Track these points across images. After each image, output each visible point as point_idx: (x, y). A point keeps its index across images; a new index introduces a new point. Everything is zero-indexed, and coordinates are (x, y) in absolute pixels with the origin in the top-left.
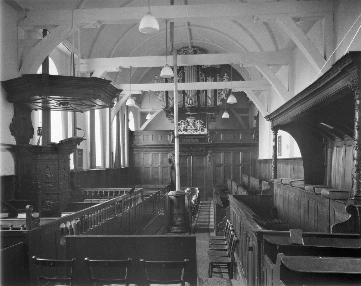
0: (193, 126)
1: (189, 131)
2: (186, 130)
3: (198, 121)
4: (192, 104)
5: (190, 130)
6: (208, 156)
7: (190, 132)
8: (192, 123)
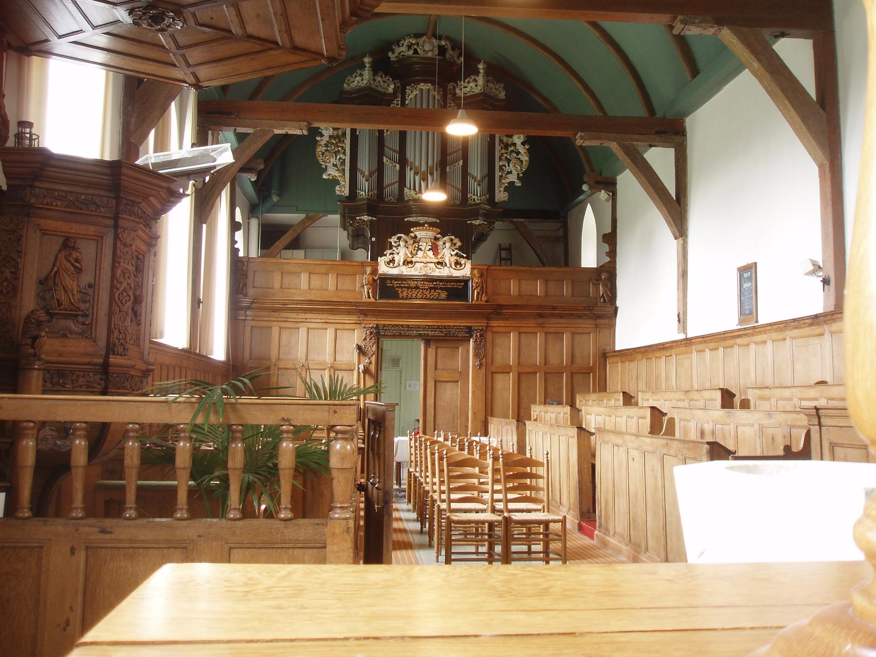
0: (431, 253)
2: (411, 262)
3: (446, 238)
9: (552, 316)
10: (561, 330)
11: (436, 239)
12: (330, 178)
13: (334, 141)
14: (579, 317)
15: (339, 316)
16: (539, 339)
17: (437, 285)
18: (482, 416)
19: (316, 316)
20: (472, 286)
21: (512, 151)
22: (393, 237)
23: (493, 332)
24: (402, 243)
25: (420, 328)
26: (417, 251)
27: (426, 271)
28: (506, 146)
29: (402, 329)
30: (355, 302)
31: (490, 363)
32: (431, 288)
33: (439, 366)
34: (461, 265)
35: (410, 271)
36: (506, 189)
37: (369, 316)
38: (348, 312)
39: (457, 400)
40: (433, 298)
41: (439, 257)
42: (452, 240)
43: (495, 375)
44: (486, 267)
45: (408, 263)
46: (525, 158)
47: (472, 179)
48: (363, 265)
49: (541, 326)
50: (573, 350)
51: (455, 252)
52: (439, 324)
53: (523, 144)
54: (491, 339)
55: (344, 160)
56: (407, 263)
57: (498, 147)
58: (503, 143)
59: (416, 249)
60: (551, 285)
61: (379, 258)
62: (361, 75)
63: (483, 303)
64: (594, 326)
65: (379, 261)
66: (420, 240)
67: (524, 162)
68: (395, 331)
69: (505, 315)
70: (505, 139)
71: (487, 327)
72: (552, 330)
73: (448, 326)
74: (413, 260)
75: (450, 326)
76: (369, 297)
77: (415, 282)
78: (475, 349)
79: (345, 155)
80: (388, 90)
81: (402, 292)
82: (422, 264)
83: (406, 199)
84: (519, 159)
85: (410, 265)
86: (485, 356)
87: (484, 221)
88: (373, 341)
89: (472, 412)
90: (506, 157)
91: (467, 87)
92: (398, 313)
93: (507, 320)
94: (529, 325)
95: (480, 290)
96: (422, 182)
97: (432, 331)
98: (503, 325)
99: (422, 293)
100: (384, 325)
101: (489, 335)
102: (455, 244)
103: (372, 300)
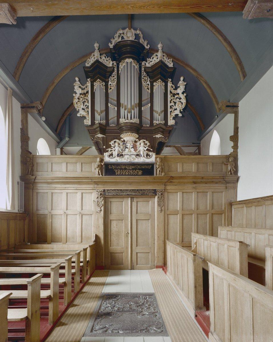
0: (132, 150)
1: (126, 157)
2: (122, 155)
3: (141, 141)
6: (156, 197)
8: (132, 144)
9: (201, 182)
10: (205, 190)
11: (136, 142)
12: (81, 116)
13: (82, 96)
14: (216, 183)
15: (84, 185)
16: (194, 196)
18: (162, 238)
19: (71, 186)
20: (156, 167)
21: (177, 98)
22: (112, 141)
24: (116, 144)
27: (130, 160)
28: (174, 95)
30: (91, 177)
31: (167, 209)
32: (133, 169)
34: (150, 156)
35: (122, 160)
36: (174, 118)
38: (88, 183)
39: (149, 229)
41: (138, 151)
42: (144, 142)
43: (169, 216)
44: (164, 157)
45: (120, 155)
46: (184, 101)
47: (156, 113)
48: (96, 157)
49: (195, 188)
50: (213, 201)
51: (146, 148)
52: (138, 189)
53: (183, 93)
54: (167, 197)
55: (88, 106)
56: (120, 155)
57: (169, 96)
58: (172, 93)
59: (124, 147)
60: (201, 165)
61: (104, 153)
62: (94, 55)
63: (163, 176)
64: (225, 188)
65: (104, 155)
66: (127, 143)
67: (183, 104)
68: (114, 193)
70: (173, 91)
72: (201, 191)
74: (123, 153)
78: (158, 202)
79: (88, 103)
80: (109, 65)
81: (117, 171)
82: (128, 156)
84: (181, 102)
85: (121, 157)
86: (164, 205)
88: (102, 198)
89: (157, 236)
90: (174, 101)
91: (152, 61)
93: (176, 185)
94: (188, 188)
96: (128, 113)
97: (134, 193)
98: (174, 188)
99: (129, 171)
100: (108, 190)
101: (166, 194)
102: (146, 144)
103: (101, 176)
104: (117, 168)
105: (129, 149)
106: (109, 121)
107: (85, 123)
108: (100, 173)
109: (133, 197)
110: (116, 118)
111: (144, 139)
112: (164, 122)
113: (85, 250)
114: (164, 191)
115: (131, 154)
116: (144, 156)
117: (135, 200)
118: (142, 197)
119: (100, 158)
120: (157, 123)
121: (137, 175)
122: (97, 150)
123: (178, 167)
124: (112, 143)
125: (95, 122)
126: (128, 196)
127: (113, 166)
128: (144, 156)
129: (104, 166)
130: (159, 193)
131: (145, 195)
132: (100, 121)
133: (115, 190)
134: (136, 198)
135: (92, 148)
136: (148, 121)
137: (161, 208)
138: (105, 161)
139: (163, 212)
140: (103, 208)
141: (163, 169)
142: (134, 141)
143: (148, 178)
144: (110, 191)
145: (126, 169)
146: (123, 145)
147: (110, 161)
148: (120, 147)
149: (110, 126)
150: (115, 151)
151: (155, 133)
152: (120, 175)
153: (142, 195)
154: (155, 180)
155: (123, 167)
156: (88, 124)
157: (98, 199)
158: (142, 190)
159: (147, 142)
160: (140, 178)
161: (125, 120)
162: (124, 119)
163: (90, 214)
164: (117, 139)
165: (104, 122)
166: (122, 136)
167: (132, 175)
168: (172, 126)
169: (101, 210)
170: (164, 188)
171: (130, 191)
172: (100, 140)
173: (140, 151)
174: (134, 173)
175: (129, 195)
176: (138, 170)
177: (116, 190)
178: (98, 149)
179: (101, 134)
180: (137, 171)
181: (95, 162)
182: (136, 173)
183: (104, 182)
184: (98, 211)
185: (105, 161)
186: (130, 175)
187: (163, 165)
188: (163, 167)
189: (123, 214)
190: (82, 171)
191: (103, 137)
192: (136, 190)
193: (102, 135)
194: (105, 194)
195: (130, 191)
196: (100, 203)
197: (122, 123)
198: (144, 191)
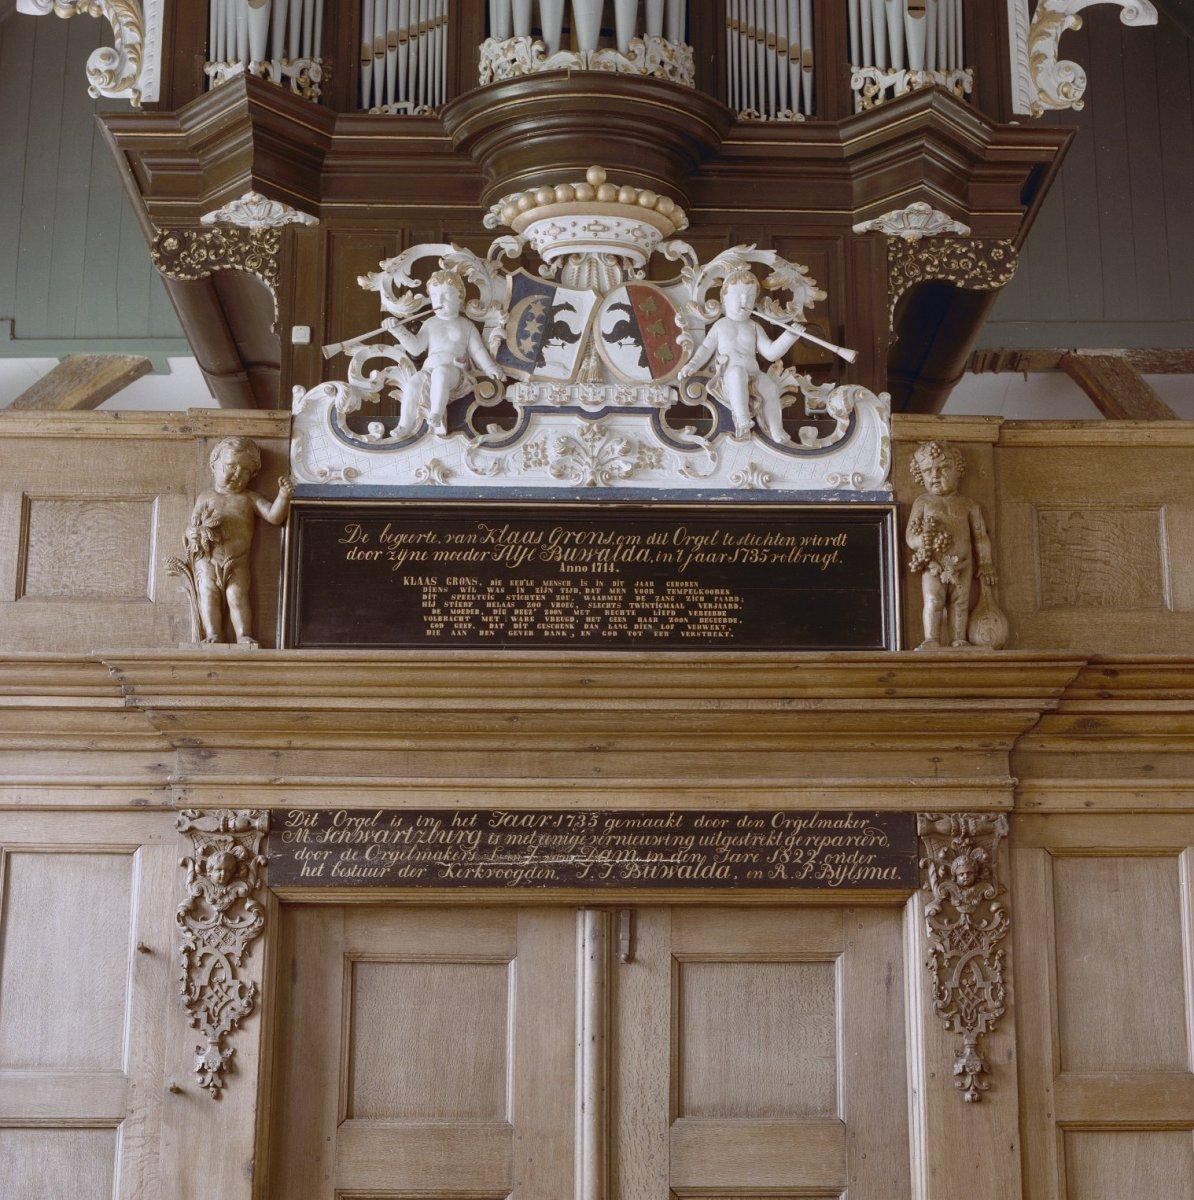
0: (625, 356)
1: (549, 431)
2: (504, 414)
3: (727, 260)
4: (607, 35)
5: (566, 410)
6: (914, 907)
7: (569, 447)
8: (622, 296)
11: (661, 269)
17: (670, 548)
20: (905, 552)
23: (1056, 855)
24: (439, 292)
25: (564, 829)
26: (543, 340)
27: (599, 465)
29: (446, 837)
32: (630, 573)
33: (697, 1091)
34: (825, 424)
36: (1070, 46)
37: (223, 760)
40: (648, 635)
41: (683, 372)
42: (760, 271)
43: (1081, 1143)
44: (990, 433)
45: (483, 417)
48: (193, 432)
51: (785, 342)
59: (533, 327)
65: (297, 407)
66: (558, 278)
68: (394, 857)
69: (1132, 735)
71: (1011, 815)
73: (753, 815)
74: (517, 395)
75: (766, 815)
76: (225, 634)
77: (529, 537)
78: (939, 966)
81: (441, 599)
82: (576, 421)
83: (483, 80)
86: (1011, 1011)
87: (956, 216)
92: (418, 734)
93: (1148, 770)
95: (959, 573)
99: (579, 601)
100: (325, 818)
101: (1031, 874)
103: (244, 645)
104: (438, 556)
105: (586, 352)
106: (366, 71)
107: (99, 87)
108: (236, 617)
109: (633, 910)
110: (437, 42)
111: (762, 247)
112: (968, 77)
113: (112, 130)
114: (1009, 839)
115: (613, 403)
116: (757, 430)
117: (655, 940)
118: (745, 907)
119: (247, 444)
120: (890, 91)
121: (675, 642)
122: (224, 373)
123: (1165, 563)
124: (386, 279)
125: (210, 71)
126: (571, 895)
127: (394, 531)
128: (757, 430)
129: (286, 532)
130: (950, 856)
131: (779, 884)
132: (268, 56)
133: (409, 816)
134: (665, 917)
135: (167, 371)
136: (795, 68)
137: (976, 1047)
138: (299, 477)
139: (1006, 1097)
140: (249, 1044)
141: (988, 577)
142: (640, 262)
143: (808, 676)
144: (345, 836)
145: (552, 571)
146: (514, 301)
147: (360, 481)
148: (480, 326)
149: (376, 110)
150: (427, 364)
151: (873, 191)
152: (472, 641)
153: (740, 878)
154: (891, 696)
155: (515, 549)
156: (128, 94)
157: (199, 925)
158: (743, 823)
159: (788, 274)
160: (712, 678)
161: (538, 47)
162: (524, 51)
163: (77, 1109)
164: (446, 241)
165: (305, 70)
166: (501, 212)
167: (622, 642)
168: (1057, 120)
169: (228, 1069)
170: (1007, 801)
171: (599, 830)
172: (251, 265)
173: (708, 366)
174: (647, 613)
175: (584, 884)
176: (689, 589)
177: (427, 813)
178: (232, 364)
179: (270, 194)
180: (680, 599)
181: (187, 491)
182: (664, 620)
183: (280, 719)
184: (193, 1083)
185: (299, 477)
186: (597, 642)
187: (979, 525)
188: (984, 548)
189: (509, 1116)
190: (20, 591)
191: (292, 227)
192: (664, 815)
193: (277, 206)
194: (286, 869)
195: (599, 830)
196: (224, 974)
197: (501, 76)
198: (766, 830)
